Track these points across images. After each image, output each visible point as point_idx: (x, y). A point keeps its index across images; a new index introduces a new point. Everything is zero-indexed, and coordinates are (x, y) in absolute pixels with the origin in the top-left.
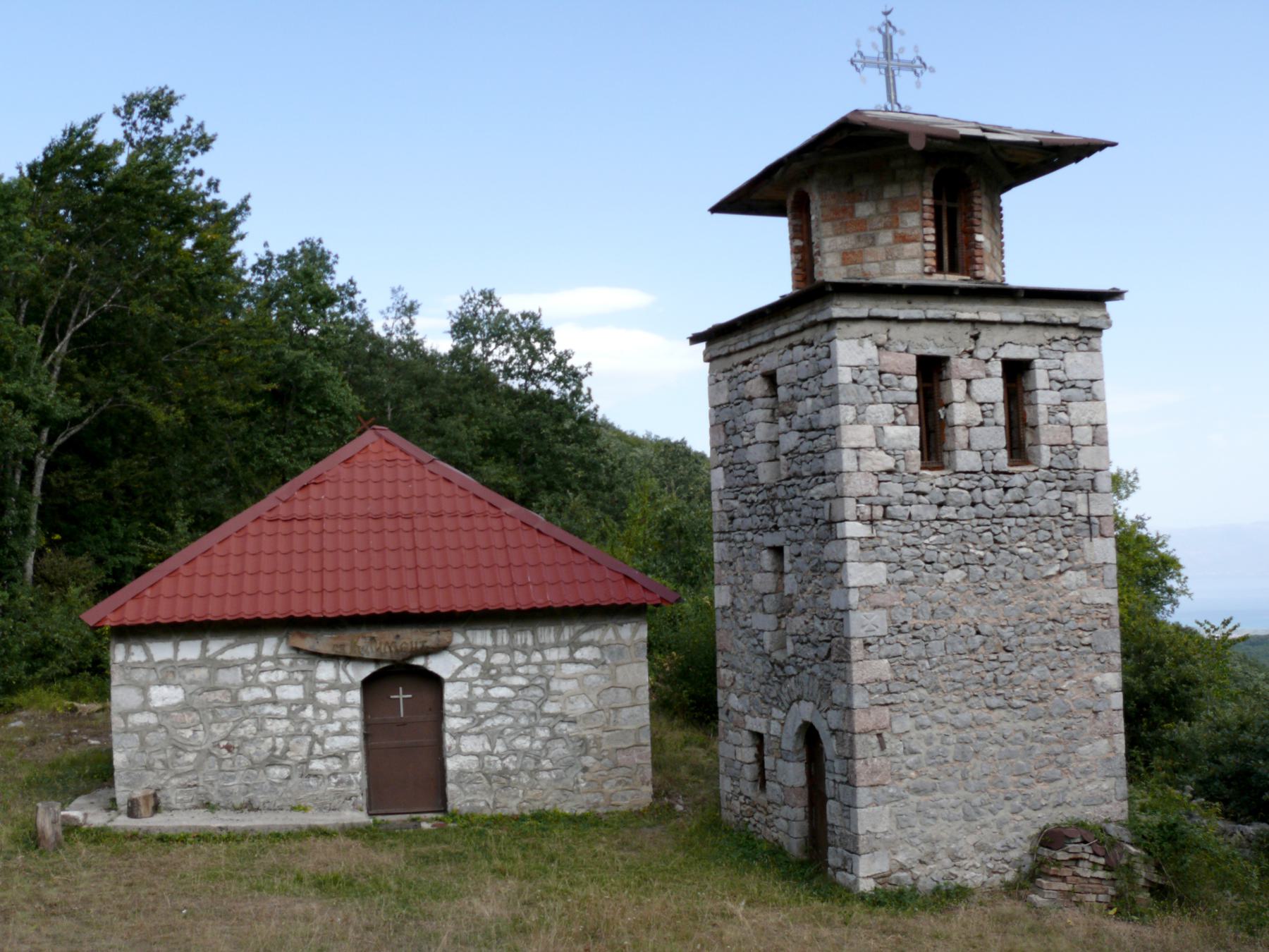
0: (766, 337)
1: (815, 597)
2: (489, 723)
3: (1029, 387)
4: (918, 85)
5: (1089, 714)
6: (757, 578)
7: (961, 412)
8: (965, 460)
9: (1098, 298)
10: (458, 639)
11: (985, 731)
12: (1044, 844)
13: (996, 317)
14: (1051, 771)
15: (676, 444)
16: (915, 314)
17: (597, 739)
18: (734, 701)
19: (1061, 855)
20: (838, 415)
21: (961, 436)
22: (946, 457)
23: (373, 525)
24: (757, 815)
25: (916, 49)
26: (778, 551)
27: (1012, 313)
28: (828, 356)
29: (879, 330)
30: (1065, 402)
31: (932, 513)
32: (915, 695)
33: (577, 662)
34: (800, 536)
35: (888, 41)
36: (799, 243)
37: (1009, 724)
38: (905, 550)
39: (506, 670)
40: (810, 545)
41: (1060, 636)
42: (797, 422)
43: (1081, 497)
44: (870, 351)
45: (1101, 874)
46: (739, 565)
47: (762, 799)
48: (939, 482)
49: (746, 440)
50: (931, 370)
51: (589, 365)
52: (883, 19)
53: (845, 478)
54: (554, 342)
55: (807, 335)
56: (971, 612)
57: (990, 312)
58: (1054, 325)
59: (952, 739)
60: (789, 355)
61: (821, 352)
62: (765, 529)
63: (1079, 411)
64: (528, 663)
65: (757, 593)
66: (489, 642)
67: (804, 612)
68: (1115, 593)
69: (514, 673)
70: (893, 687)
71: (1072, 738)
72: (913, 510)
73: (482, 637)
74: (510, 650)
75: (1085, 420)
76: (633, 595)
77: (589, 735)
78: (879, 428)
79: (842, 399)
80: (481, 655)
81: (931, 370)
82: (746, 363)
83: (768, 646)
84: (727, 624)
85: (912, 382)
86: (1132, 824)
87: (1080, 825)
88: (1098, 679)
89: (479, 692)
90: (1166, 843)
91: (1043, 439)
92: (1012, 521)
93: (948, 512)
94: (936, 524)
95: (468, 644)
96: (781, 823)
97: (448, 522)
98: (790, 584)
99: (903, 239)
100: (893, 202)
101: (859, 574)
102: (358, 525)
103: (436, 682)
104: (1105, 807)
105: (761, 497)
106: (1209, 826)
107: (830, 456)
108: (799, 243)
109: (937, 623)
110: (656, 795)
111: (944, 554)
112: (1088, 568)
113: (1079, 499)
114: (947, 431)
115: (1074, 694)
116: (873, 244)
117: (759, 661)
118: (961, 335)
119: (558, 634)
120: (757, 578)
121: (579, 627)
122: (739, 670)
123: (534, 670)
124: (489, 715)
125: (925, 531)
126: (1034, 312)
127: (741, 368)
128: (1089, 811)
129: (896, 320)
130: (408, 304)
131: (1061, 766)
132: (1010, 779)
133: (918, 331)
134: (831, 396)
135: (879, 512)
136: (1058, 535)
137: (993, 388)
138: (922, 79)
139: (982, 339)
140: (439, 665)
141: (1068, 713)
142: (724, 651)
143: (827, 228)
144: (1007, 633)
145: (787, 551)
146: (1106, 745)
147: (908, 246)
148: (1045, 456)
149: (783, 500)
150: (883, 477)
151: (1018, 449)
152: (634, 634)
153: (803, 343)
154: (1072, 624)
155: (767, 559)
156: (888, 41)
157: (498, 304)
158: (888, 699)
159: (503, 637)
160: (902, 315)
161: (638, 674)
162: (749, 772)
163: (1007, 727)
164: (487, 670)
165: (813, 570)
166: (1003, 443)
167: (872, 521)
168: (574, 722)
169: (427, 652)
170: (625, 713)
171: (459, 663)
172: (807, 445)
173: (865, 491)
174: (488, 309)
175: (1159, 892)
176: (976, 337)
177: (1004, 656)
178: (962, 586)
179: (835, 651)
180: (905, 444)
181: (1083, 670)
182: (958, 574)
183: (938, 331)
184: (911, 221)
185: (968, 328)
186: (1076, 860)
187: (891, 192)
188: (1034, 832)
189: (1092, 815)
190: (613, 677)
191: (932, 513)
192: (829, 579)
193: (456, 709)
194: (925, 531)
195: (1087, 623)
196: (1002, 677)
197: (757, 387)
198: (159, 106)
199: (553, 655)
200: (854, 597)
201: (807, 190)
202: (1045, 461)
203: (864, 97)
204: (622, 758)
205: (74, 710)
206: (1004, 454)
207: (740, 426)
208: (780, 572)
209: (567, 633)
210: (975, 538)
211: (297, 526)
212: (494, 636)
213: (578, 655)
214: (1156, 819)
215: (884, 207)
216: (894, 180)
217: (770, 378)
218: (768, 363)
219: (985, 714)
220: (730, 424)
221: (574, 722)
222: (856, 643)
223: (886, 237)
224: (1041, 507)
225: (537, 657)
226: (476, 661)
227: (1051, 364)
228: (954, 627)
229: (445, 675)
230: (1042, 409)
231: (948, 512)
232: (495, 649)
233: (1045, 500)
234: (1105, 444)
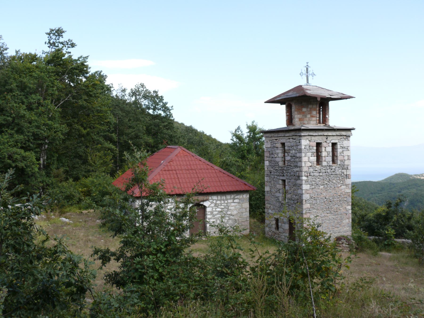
0: (283, 136)
1: (294, 191)
2: (216, 216)
4: (313, 79)
6: (278, 186)
7: (324, 154)
8: (324, 164)
9: (349, 130)
10: (210, 198)
11: (326, 218)
12: (337, 240)
13: (331, 134)
14: (338, 226)
16: (316, 134)
17: (238, 219)
18: (270, 211)
19: (340, 242)
20: (301, 155)
21: (324, 158)
22: (320, 163)
23: (188, 172)
24: (276, 235)
26: (284, 181)
27: (334, 133)
28: (299, 142)
29: (309, 137)
30: (343, 151)
31: (318, 174)
32: (314, 211)
33: (234, 203)
34: (290, 178)
35: (307, 69)
36: (288, 114)
37: (331, 216)
38: (313, 182)
39: (220, 204)
40: (293, 180)
41: (340, 199)
43: (345, 170)
44: (308, 142)
45: (347, 246)
46: (272, 182)
47: (277, 232)
48: (319, 168)
49: (275, 156)
50: (319, 145)
51: (172, 107)
53: (303, 168)
54: (163, 100)
55: (294, 137)
56: (324, 194)
57: (330, 133)
58: (341, 136)
59: (320, 219)
60: (288, 140)
62: (281, 176)
63: (346, 153)
64: (224, 203)
65: (277, 189)
66: (216, 199)
67: (291, 193)
68: (351, 190)
69: (221, 205)
70: (310, 209)
72: (315, 174)
73: (215, 197)
74: (221, 200)
75: (346, 155)
77: (236, 218)
78: (309, 158)
79: (302, 152)
80: (215, 201)
81: (319, 145)
82: (276, 140)
83: (280, 200)
84: (268, 195)
85: (315, 148)
86: (352, 236)
87: (343, 236)
88: (347, 207)
89: (214, 209)
90: (359, 240)
91: (339, 159)
92: (332, 176)
93: (321, 174)
95: (212, 199)
96: (283, 237)
97: (204, 171)
98: (287, 188)
99: (312, 117)
100: (311, 108)
101: (305, 187)
103: (205, 207)
104: (347, 233)
105: (279, 169)
106: (365, 236)
107: (299, 163)
108: (288, 114)
109: (319, 196)
110: (250, 231)
111: (320, 183)
112: (346, 185)
113: (344, 171)
114: (321, 157)
115: (343, 211)
116: (306, 117)
117: (278, 203)
118: (324, 138)
119: (231, 197)
120: (278, 186)
121: (235, 195)
122: (271, 205)
123: (225, 204)
124: (216, 215)
125: (317, 178)
126: (338, 133)
127: (275, 141)
128: (345, 234)
129: (313, 136)
130: (123, 89)
131: (340, 225)
132: (331, 227)
133: (317, 138)
134: (300, 151)
135: (308, 174)
136: (341, 178)
137: (330, 149)
138: (314, 77)
139: (328, 139)
140: (206, 204)
141: (341, 214)
142: (267, 200)
143: (296, 113)
144: (331, 198)
145: (286, 181)
146: (348, 221)
147: (313, 118)
148: (339, 162)
149: (286, 170)
150: (310, 167)
151: (334, 161)
152: (246, 196)
153: (293, 139)
154: (343, 196)
155: (281, 182)
156: (307, 69)
157: (145, 88)
158: (309, 212)
159: (219, 197)
160: (314, 134)
161: (247, 205)
162: (274, 226)
163: (330, 217)
164: (216, 205)
165: (294, 185)
166: (331, 160)
167: (307, 176)
169: (203, 201)
170: (244, 214)
175: (357, 248)
176: (327, 138)
177: (330, 203)
178: (323, 189)
179: (300, 201)
180: (313, 161)
181: (345, 206)
182: (322, 187)
183: (320, 138)
185: (326, 137)
186: (343, 243)
187: (310, 106)
188: (334, 238)
189: (345, 234)
190: (242, 206)
191: (318, 174)
192: (298, 187)
193: (209, 213)
194: (317, 178)
195: (345, 196)
196: (330, 207)
197: (279, 145)
198: (59, 32)
199: (229, 201)
200: (304, 192)
201: (291, 103)
202: (339, 164)
203: (302, 82)
205: (82, 212)
206: (331, 162)
207: (274, 153)
208: (285, 185)
210: (325, 179)
211: (171, 172)
212: (217, 197)
213: (235, 201)
214: (357, 235)
215: (309, 109)
216: (311, 104)
217: (283, 144)
218: (283, 141)
219: (326, 214)
220: (271, 152)
221: (233, 216)
222: (304, 201)
223: (309, 116)
224: (338, 173)
225: (226, 202)
226: (213, 203)
227: (341, 144)
228: (321, 197)
229: (207, 206)
230: (339, 153)
231: (321, 174)
232: (217, 200)
233: (339, 171)
234: (350, 160)
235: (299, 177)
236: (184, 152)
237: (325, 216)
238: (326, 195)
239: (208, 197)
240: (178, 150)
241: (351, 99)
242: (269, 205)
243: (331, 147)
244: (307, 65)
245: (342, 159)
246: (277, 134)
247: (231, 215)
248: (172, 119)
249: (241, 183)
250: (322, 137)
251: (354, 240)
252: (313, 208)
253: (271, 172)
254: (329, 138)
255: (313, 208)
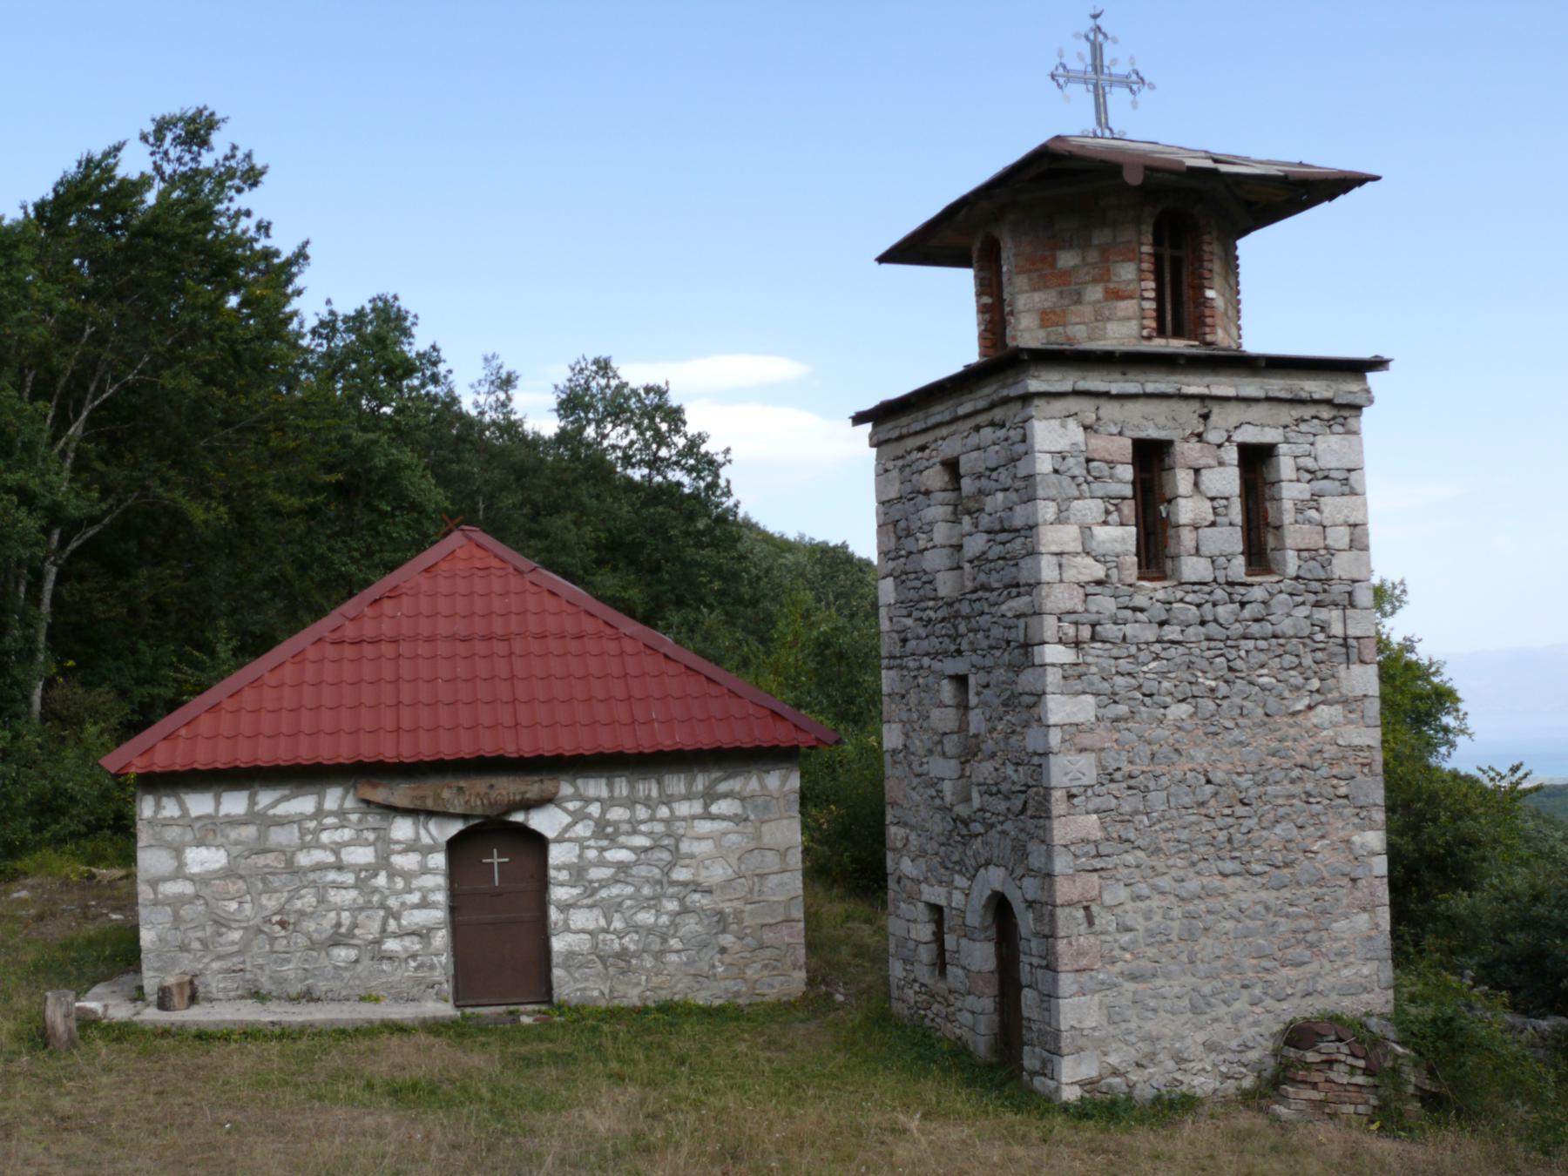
0: (947, 416)
1: (1007, 737)
2: (604, 893)
3: (1272, 477)
4: (1135, 105)
5: (1345, 881)
6: (936, 713)
7: (1188, 509)
8: (1193, 568)
9: (1357, 368)
10: (566, 789)
11: (1216, 903)
12: (1290, 1042)
13: (1231, 392)
14: (1299, 952)
15: (836, 547)
16: (1131, 387)
17: (738, 913)
18: (907, 866)
19: (1311, 1057)
20: (1035, 513)
21: (1187, 538)
22: (1169, 564)
23: (461, 648)
24: (935, 1007)
25: (1132, 60)
26: (961, 681)
27: (1251, 387)
28: (1024, 440)
29: (1086, 408)
30: (1316, 496)
31: (1151, 633)
32: (1130, 859)
33: (713, 818)
34: (989, 662)
35: (1097, 51)
36: (987, 300)
37: (1247, 895)
38: (1119, 680)
39: (625, 827)
40: (1001, 674)
41: (1309, 786)
42: (985, 521)
43: (1336, 614)
44: (1075, 433)
45: (1360, 1080)
46: (912, 698)
47: (942, 987)
48: (1160, 595)
49: (922, 544)
50: (1151, 457)
51: (727, 451)
52: (1091, 23)
53: (1045, 590)
54: (684, 423)
55: (998, 414)
57: (1223, 386)
59: (1177, 913)
60: (974, 439)
61: (1015, 435)
62: (946, 653)
63: (1334, 508)
64: (652, 819)
65: (935, 732)
66: (604, 793)
67: (993, 755)
68: (1378, 733)
69: (635, 832)
70: (1103, 849)
71: (1324, 912)
72: (1129, 629)
73: (595, 787)
74: (631, 803)
75: (1340, 518)
76: (782, 735)
77: (727, 907)
78: (1086, 529)
79: (1041, 493)
80: (595, 810)
81: (1151, 457)
82: (922, 449)
83: (948, 799)
84: (899, 771)
85: (1127, 472)
86: (1398, 1018)
87: (1335, 1019)
88: (1356, 839)
89: (592, 854)
90: (1440, 1042)
91: (1289, 542)
92: (1250, 644)
93: (1172, 632)
94: (1157, 648)
95: (578, 796)
98: (976, 721)
99: (1116, 295)
100: (1104, 250)
101: (1061, 709)
102: (443, 648)
103: (539, 843)
104: (1365, 997)
105: (940, 614)
106: (1494, 1020)
107: (1025, 564)
108: (987, 300)
109: (1158, 770)
110: (810, 982)
111: (1166, 684)
112: (1344, 701)
114: (1171, 532)
115: (1327, 857)
116: (1079, 302)
117: (938, 817)
118: (1188, 414)
119: (690, 784)
120: (936, 713)
121: (716, 775)
122: (913, 828)
123: (659, 828)
124: (604, 884)
125: (1143, 656)
126: (1277, 385)
127: (916, 455)
129: (1107, 395)
130: (504, 376)
131: (1311, 946)
133: (1134, 410)
134: (1027, 489)
135: (1086, 632)
136: (1308, 661)
137: (1226, 480)
138: (1139, 97)
139: (1214, 418)
140: (543, 821)
141: (1320, 881)
142: (894, 804)
143: (1022, 281)
144: (1244, 781)
145: (972, 680)
146: (1366, 921)
147: (1122, 304)
148: (1292, 563)
149: (968, 618)
150: (1091, 589)
151: (1258, 554)
152: (783, 783)
153: (992, 424)
154: (1324, 771)
155: (947, 690)
156: (1097, 51)
157: (615, 376)
158: (1098, 863)
159: (622, 787)
160: (1115, 389)
161: (788, 832)
162: (926, 954)
163: (1245, 898)
164: (606, 832)
165: (1005, 704)
168: (709, 891)
169: (528, 805)
170: (773, 881)
171: (567, 819)
172: (997, 550)
173: (1068, 605)
174: (603, 382)
175: (1432, 1102)
176: (1205, 417)
177: (1240, 810)
178: (1189, 724)
179: (1031, 804)
180: (1119, 548)
181: (1338, 828)
182: (1184, 709)
183: (1159, 409)
184: (1126, 272)
185: (1196, 406)
186: (1330, 1063)
187: (1100, 237)
188: (1278, 1028)
189: (1349, 1006)
190: (758, 836)
191: (1151, 633)
192: (1025, 715)
193: (563, 876)
194: (1143, 656)
195: (1343, 769)
196: (1238, 837)
197: (935, 478)
199: (683, 809)
200: (1055, 738)
202: (1292, 569)
203: (1068, 119)
204: (768, 936)
205: (92, 876)
207: (914, 526)
208: (964, 707)
209: (701, 782)
211: (368, 650)
212: (610, 786)
213: (714, 809)
214: (1429, 1012)
215: (1093, 256)
218: (948, 449)
219: (1217, 882)
220: (902, 524)
221: (709, 891)
222: (1058, 795)
223: (1095, 293)
224: (1286, 626)
225: (663, 812)
226: (588, 817)
227: (1299, 450)
228: (1178, 775)
229: (550, 834)
230: (1288, 505)
231: (1172, 632)
232: (611, 802)
233: (1291, 618)
234: (1365, 548)
235: (1025, 650)
236: (479, 553)
237: (1207, 893)
238: (1214, 763)
239: (548, 786)
240: (460, 548)
241: (1356, 191)
242: (902, 832)
243: (1236, 471)
244: (1098, 29)
245: (1314, 540)
246: (921, 415)
247: (696, 886)
248: (729, 503)
249: (751, 710)
250: (1175, 405)
251: (1403, 1044)
252: (1122, 840)
253: (904, 641)
254: (1223, 417)
255: (1122, 840)
